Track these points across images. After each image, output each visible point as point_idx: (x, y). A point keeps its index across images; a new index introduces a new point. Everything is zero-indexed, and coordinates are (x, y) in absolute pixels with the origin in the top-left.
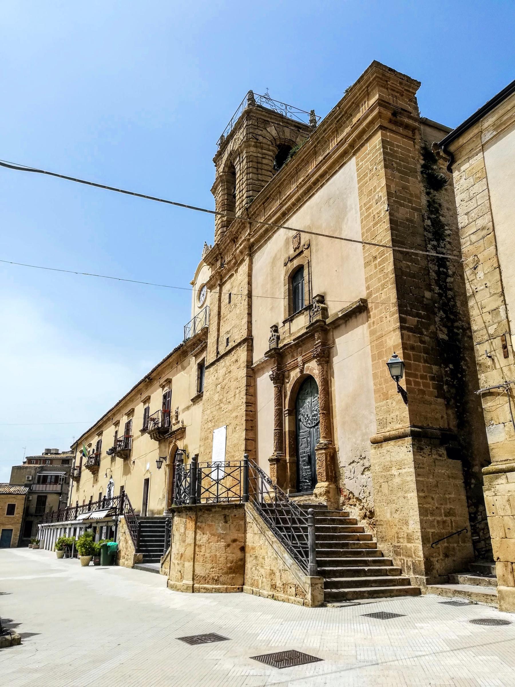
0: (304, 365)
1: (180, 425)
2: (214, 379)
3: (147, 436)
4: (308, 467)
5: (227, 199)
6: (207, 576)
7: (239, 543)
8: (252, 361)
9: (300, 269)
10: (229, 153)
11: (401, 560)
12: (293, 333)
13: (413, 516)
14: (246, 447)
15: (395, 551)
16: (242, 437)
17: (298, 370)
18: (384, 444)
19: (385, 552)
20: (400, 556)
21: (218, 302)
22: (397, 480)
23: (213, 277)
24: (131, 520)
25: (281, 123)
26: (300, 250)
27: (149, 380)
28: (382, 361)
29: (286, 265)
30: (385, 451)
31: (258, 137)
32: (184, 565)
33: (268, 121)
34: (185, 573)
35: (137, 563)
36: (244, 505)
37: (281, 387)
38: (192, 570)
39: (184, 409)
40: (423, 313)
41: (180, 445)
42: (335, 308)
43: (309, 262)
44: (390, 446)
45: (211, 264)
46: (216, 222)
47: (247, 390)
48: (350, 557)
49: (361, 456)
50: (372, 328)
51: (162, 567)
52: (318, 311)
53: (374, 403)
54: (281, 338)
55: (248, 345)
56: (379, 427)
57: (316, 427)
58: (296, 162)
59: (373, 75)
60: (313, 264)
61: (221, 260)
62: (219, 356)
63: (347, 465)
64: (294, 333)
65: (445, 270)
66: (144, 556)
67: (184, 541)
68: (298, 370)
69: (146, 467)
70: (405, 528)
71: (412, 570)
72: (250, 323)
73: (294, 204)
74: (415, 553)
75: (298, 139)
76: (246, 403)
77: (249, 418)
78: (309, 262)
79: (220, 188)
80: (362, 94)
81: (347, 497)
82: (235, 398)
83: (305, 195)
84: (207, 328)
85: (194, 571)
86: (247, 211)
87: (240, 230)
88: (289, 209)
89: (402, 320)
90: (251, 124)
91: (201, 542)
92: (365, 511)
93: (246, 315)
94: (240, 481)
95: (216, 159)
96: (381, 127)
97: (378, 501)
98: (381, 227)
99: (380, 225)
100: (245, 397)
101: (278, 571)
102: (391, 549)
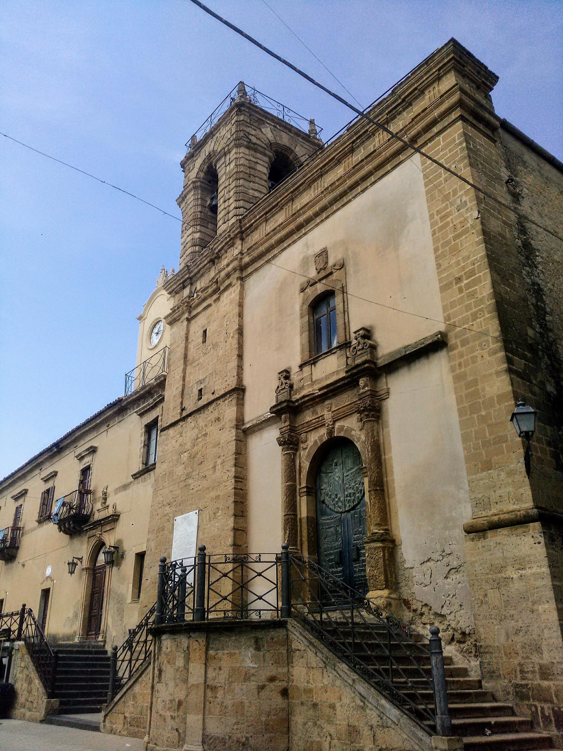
0: (334, 424)
1: (110, 511)
2: (177, 445)
3: (51, 528)
4: (340, 569)
5: (201, 212)
6: (227, 737)
7: (280, 684)
8: (243, 420)
9: (328, 295)
10: (207, 154)
11: (530, 707)
12: (316, 380)
13: (551, 638)
14: (234, 541)
15: (517, 693)
16: (228, 525)
17: (323, 431)
18: (490, 534)
19: (500, 694)
20: (529, 700)
21: (184, 342)
22: (517, 586)
23: (178, 308)
24: (30, 647)
25: (278, 126)
26: (328, 271)
27: (57, 449)
28: (477, 416)
29: (303, 290)
30: (492, 544)
31: (250, 137)
32: (185, 718)
33: (262, 120)
34: (188, 733)
35: (51, 717)
36: (286, 622)
37: (295, 455)
38: (201, 727)
39: (117, 489)
40: (529, 355)
41: (110, 540)
42: (389, 345)
43: (343, 287)
44: (501, 536)
45: (173, 293)
46: (183, 240)
47: (236, 459)
48: (456, 703)
49: (444, 551)
50: (458, 371)
51: (104, 721)
52: (363, 348)
53: (465, 474)
54: (295, 387)
55: (238, 398)
56: (476, 510)
57: (352, 512)
58: (322, 162)
59: (448, 55)
60: (351, 289)
61: (191, 289)
62: (184, 414)
63: (417, 565)
64: (321, 380)
65: (542, 305)
66: (61, 703)
67: (186, 681)
68: (323, 431)
69: (44, 573)
70: (535, 658)
71: (553, 722)
72: (240, 367)
73: (317, 215)
74: (556, 696)
75: (297, 148)
76: (235, 477)
77: (239, 500)
78: (343, 287)
79: (191, 197)
80: (429, 79)
81: (418, 612)
82: (215, 471)
83: (336, 202)
84: (165, 376)
85: (204, 729)
86: (240, 222)
87: (226, 247)
88: (308, 221)
89: (509, 361)
90: (243, 120)
91: (216, 681)
92: (451, 632)
93: (235, 357)
94: (277, 585)
95: (185, 163)
96: (461, 118)
97: (481, 617)
98: (468, 239)
99: (466, 237)
100: (233, 469)
101: (366, 728)
102: (511, 690)
